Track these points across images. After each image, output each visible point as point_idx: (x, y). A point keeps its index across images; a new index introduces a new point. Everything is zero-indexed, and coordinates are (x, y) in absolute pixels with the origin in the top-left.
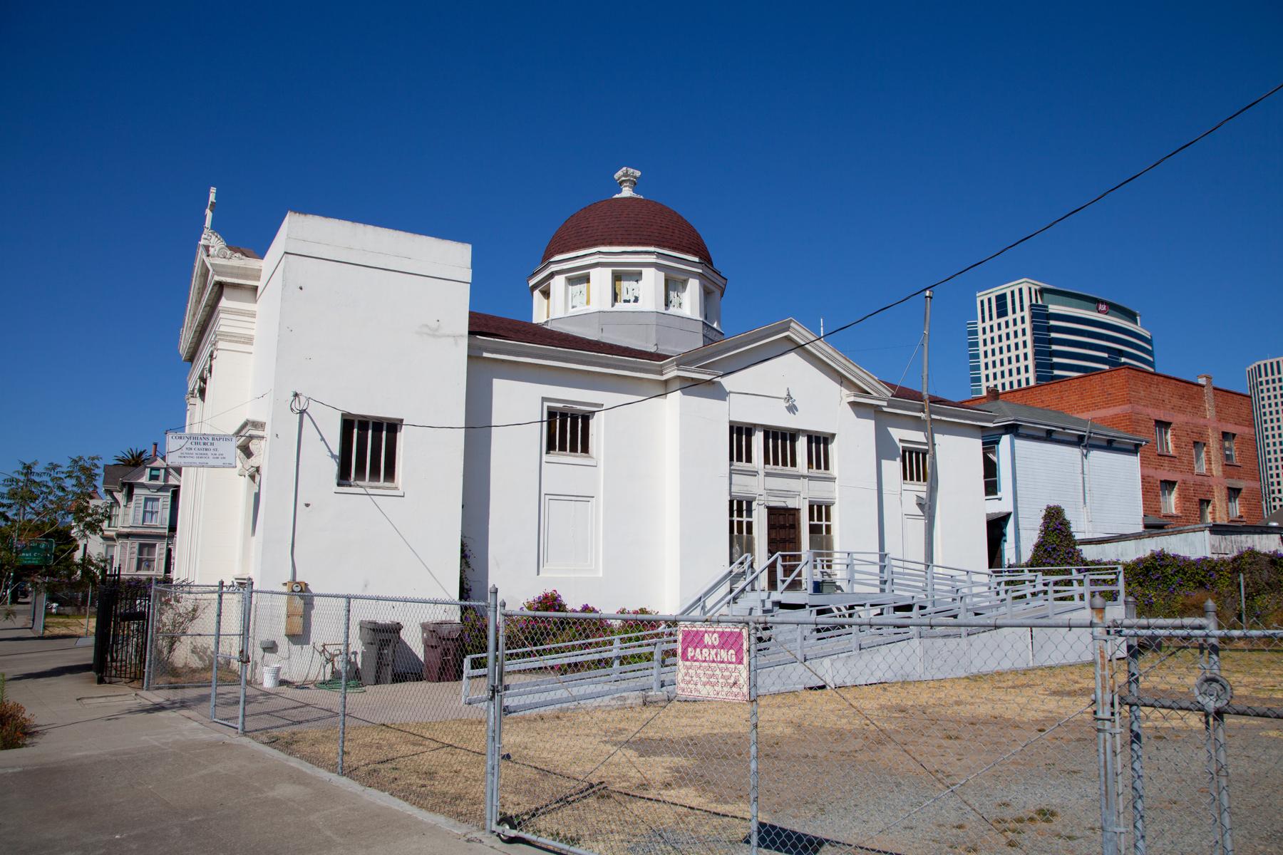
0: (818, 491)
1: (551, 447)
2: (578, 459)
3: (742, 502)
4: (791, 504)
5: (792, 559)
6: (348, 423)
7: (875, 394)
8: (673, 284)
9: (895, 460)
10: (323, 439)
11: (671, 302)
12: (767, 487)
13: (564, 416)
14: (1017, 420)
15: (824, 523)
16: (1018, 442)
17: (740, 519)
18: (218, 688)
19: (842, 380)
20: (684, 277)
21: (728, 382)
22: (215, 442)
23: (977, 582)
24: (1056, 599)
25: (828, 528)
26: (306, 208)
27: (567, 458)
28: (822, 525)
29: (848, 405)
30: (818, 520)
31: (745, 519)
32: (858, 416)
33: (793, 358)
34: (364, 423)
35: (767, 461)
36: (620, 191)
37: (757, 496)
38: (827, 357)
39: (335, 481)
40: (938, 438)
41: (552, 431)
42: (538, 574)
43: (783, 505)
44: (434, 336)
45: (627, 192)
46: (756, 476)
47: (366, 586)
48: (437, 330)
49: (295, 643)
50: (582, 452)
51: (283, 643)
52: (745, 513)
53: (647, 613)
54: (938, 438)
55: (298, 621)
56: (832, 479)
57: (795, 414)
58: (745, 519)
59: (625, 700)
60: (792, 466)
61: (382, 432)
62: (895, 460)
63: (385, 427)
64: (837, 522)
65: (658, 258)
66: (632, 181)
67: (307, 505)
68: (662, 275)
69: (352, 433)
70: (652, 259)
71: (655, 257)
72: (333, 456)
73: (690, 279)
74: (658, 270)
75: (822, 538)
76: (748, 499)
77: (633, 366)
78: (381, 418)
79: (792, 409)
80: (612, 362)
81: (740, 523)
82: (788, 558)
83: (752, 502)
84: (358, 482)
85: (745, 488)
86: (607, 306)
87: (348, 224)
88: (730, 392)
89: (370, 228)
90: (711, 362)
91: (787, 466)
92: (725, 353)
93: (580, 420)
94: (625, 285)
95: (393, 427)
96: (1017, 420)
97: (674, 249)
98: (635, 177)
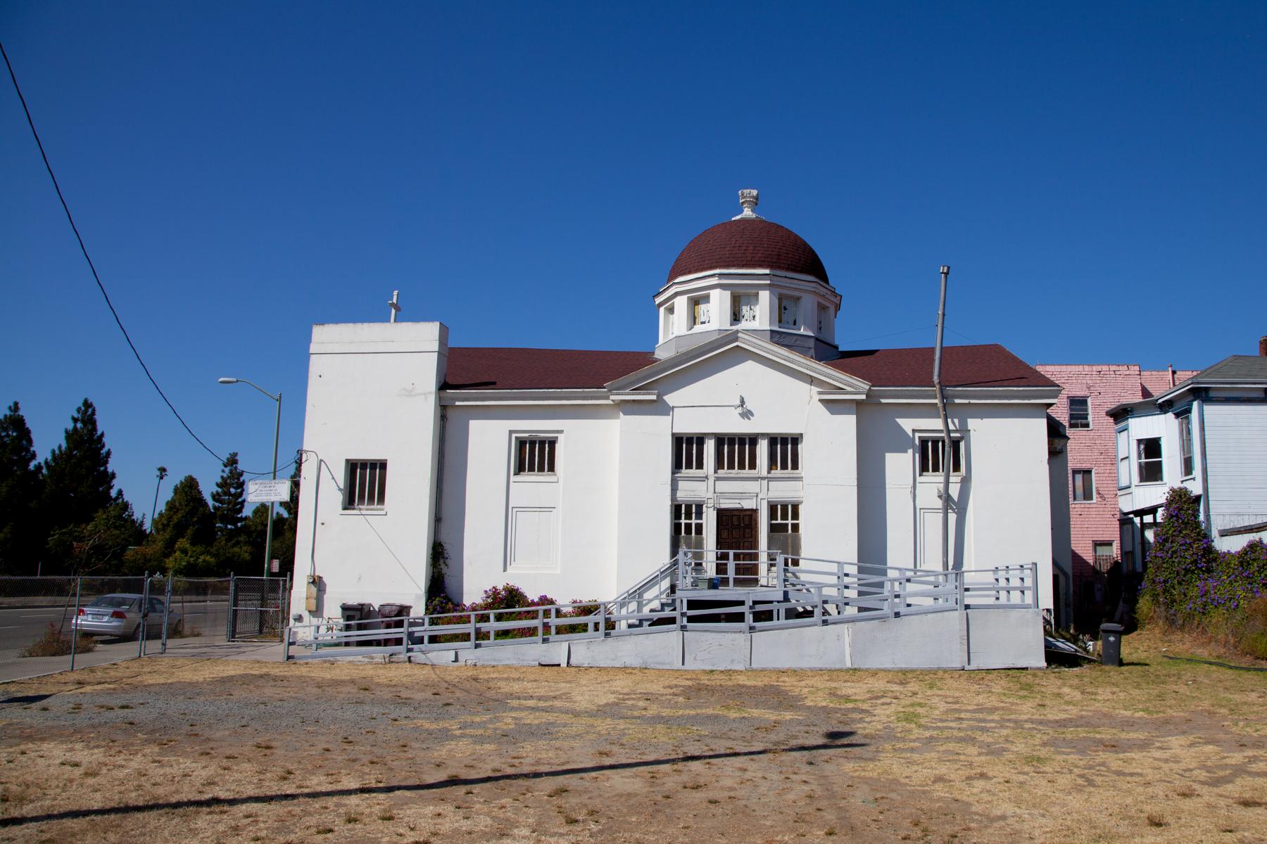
0: (782, 491)
1: (520, 469)
2: (545, 477)
3: (691, 505)
4: (748, 504)
5: (747, 557)
7: (849, 389)
9: (906, 452)
10: (333, 478)
11: (743, 317)
13: (533, 443)
14: (1198, 383)
15: (790, 522)
16: (1208, 409)
17: (688, 521)
18: (290, 647)
19: (812, 381)
20: (754, 291)
21: (670, 399)
22: (276, 485)
25: (796, 528)
26: (322, 323)
28: (787, 525)
29: (819, 403)
30: (782, 519)
31: (694, 521)
32: (833, 413)
33: (750, 365)
34: (364, 464)
36: (742, 211)
39: (340, 507)
40: (972, 423)
41: (523, 456)
42: (505, 570)
43: (738, 506)
45: (747, 213)
46: (704, 481)
47: (360, 579)
48: (411, 391)
49: (314, 617)
50: (548, 471)
51: (306, 615)
52: (694, 515)
54: (972, 423)
55: (313, 602)
56: (799, 479)
57: (749, 419)
58: (694, 521)
59: (373, 658)
60: (792, 469)
62: (906, 452)
63: (378, 466)
65: (720, 279)
66: (750, 201)
67: (323, 524)
69: (357, 472)
70: (715, 281)
71: (717, 278)
72: (340, 489)
73: (760, 292)
74: (723, 289)
75: (786, 537)
76: (697, 503)
77: (569, 395)
78: (786, 434)
79: (747, 414)
80: (562, 395)
82: (742, 556)
83: (798, 505)
84: (360, 506)
85: (692, 493)
86: (726, 325)
87: (351, 325)
88: (673, 407)
89: (366, 325)
90: (664, 376)
91: (734, 469)
92: (662, 373)
93: (547, 445)
95: (383, 465)
96: (1198, 383)
97: (743, 266)
98: (753, 197)
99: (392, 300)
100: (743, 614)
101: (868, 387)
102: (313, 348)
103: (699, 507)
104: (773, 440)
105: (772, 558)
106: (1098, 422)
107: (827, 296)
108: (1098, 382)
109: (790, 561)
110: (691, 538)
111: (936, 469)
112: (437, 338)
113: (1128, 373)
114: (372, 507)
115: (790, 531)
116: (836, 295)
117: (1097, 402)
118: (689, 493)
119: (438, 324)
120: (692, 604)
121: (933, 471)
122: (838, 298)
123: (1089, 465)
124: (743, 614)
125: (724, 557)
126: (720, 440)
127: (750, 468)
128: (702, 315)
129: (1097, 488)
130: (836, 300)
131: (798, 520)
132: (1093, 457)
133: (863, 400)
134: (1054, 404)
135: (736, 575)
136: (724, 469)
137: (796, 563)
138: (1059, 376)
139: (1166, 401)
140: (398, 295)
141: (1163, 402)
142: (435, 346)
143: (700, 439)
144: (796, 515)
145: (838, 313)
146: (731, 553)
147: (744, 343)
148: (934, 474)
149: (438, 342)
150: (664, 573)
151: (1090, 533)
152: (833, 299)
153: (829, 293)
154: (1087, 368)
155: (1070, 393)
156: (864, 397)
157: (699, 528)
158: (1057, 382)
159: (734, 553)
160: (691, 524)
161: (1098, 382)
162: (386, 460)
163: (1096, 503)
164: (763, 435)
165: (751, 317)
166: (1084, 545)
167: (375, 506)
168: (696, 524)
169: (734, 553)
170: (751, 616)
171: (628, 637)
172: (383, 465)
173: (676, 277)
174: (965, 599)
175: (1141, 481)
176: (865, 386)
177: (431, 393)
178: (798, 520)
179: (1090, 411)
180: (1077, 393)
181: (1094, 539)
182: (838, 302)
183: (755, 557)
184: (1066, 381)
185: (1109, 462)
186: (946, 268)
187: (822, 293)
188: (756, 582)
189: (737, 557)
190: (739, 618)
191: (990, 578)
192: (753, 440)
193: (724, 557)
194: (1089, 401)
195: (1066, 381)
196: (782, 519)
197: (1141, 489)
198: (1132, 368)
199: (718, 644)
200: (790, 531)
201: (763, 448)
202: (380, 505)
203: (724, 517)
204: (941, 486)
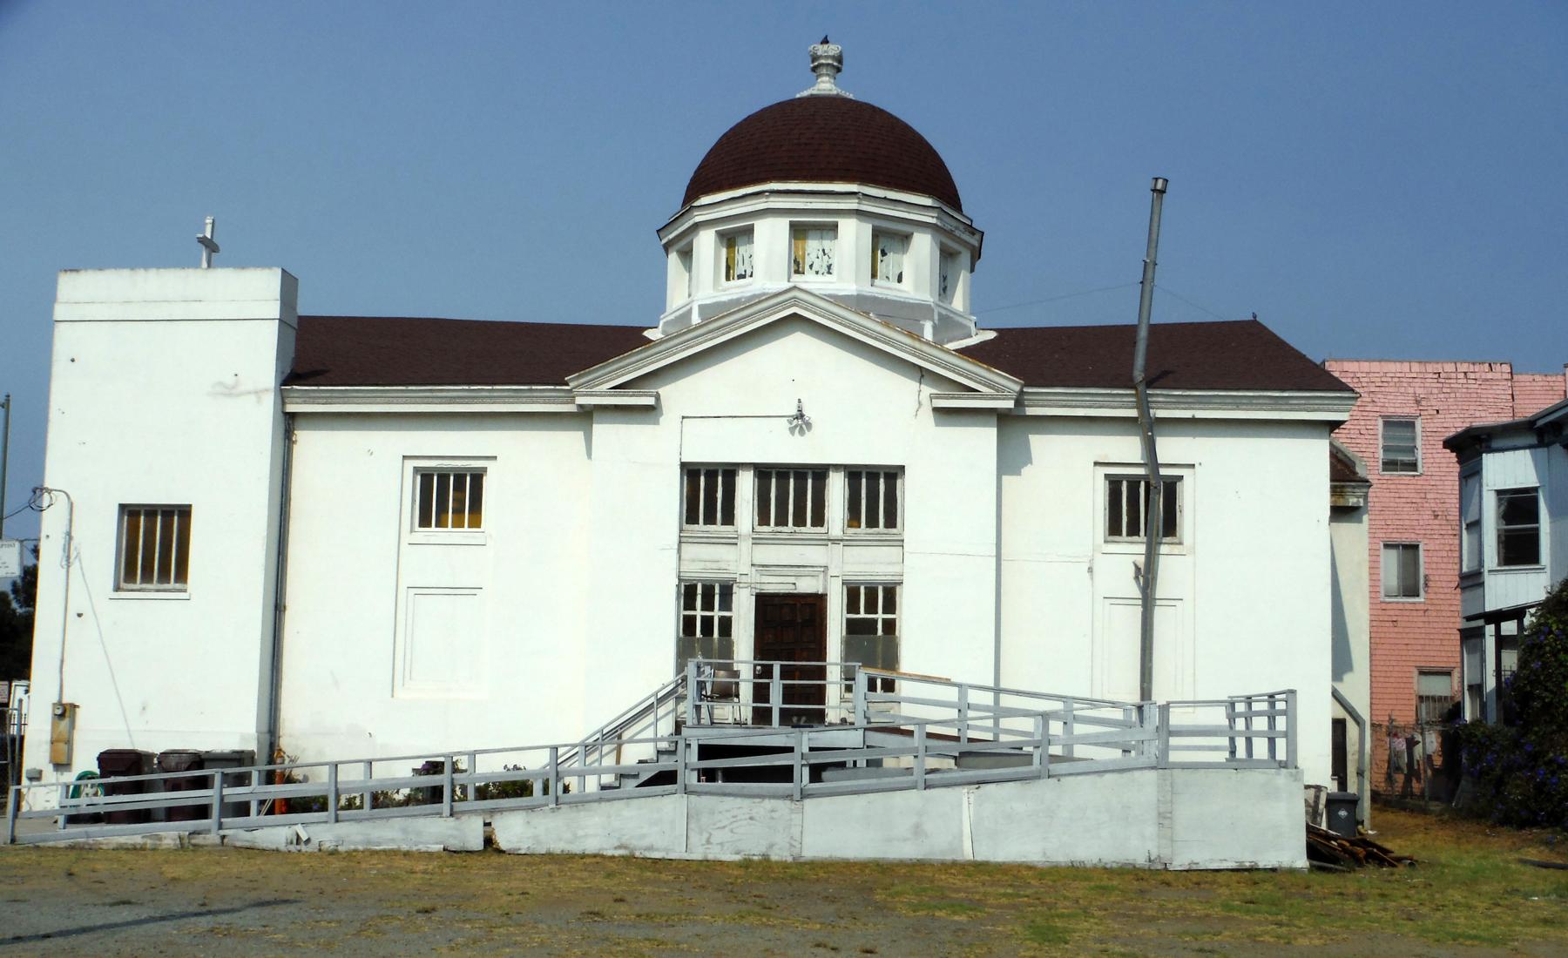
2: (465, 534)
4: (806, 586)
6: (130, 513)
8: (887, 238)
12: (755, 562)
15: (880, 616)
23: (1174, 731)
24: (790, 750)
25: (890, 626)
27: (449, 534)
30: (866, 612)
31: (717, 614)
34: (151, 511)
35: (764, 519)
37: (737, 576)
38: (875, 339)
44: (230, 395)
47: (144, 709)
53: (520, 769)
58: (717, 614)
60: (886, 526)
61: (879, 480)
64: (911, 618)
67: (80, 615)
68: (867, 229)
69: (173, 520)
70: (852, 204)
81: (707, 622)
85: (715, 566)
87: (126, 273)
89: (153, 273)
91: (805, 525)
94: (813, 246)
95: (185, 512)
99: (203, 231)
100: (790, 769)
101: (1017, 388)
102: (60, 312)
103: (727, 591)
104: (854, 474)
105: (849, 676)
106: (1432, 461)
107: (957, 233)
108: (1435, 391)
109: (879, 682)
110: (712, 640)
111: (1133, 530)
112: (279, 297)
113: (1490, 376)
114: (166, 586)
115: (880, 632)
116: (972, 230)
117: (1432, 426)
118: (709, 565)
119: (279, 272)
120: (706, 752)
121: (1129, 534)
122: (977, 237)
123: (1413, 536)
124: (790, 769)
125: (767, 672)
126: (763, 472)
127: (814, 525)
128: (741, 262)
129: (1426, 576)
130: (974, 241)
131: (894, 613)
132: (1421, 523)
133: (1010, 409)
134: (1343, 422)
135: (783, 703)
136: (769, 525)
137: (889, 686)
138: (1366, 380)
139: (1550, 422)
140: (213, 223)
141: (1546, 425)
142: (274, 310)
143: (730, 472)
144: (890, 606)
145: (978, 264)
146: (776, 667)
147: (806, 309)
148: (1130, 539)
149: (279, 302)
150: (673, 711)
151: (1410, 653)
152: (966, 237)
153: (961, 227)
154: (1416, 367)
155: (1384, 409)
156: (1010, 404)
157: (726, 625)
158: (1351, 385)
159: (781, 665)
160: (712, 617)
161: (1435, 391)
162: (190, 506)
163: (1424, 603)
164: (837, 467)
165: (825, 269)
166: (1385, 668)
167: (172, 585)
168: (722, 619)
169: (781, 665)
170: (806, 771)
171: (596, 804)
172: (185, 512)
173: (697, 198)
174: (1170, 752)
175: (1499, 565)
176: (1013, 385)
177: (267, 390)
178: (894, 613)
179: (1419, 443)
180: (1397, 410)
181: (1418, 664)
182: (977, 244)
183: (821, 673)
184: (1377, 389)
185: (1450, 532)
186: (1160, 182)
187: (948, 227)
188: (819, 717)
189: (785, 673)
190: (785, 774)
191: (1218, 717)
192: (820, 473)
193: (767, 672)
194: (1419, 424)
195: (1377, 389)
196: (866, 612)
197: (1501, 578)
198: (1497, 367)
199: (748, 816)
200: (880, 632)
201: (837, 488)
202: (181, 582)
203: (767, 604)
204: (1141, 560)
